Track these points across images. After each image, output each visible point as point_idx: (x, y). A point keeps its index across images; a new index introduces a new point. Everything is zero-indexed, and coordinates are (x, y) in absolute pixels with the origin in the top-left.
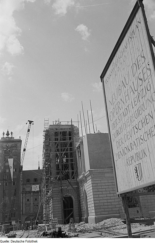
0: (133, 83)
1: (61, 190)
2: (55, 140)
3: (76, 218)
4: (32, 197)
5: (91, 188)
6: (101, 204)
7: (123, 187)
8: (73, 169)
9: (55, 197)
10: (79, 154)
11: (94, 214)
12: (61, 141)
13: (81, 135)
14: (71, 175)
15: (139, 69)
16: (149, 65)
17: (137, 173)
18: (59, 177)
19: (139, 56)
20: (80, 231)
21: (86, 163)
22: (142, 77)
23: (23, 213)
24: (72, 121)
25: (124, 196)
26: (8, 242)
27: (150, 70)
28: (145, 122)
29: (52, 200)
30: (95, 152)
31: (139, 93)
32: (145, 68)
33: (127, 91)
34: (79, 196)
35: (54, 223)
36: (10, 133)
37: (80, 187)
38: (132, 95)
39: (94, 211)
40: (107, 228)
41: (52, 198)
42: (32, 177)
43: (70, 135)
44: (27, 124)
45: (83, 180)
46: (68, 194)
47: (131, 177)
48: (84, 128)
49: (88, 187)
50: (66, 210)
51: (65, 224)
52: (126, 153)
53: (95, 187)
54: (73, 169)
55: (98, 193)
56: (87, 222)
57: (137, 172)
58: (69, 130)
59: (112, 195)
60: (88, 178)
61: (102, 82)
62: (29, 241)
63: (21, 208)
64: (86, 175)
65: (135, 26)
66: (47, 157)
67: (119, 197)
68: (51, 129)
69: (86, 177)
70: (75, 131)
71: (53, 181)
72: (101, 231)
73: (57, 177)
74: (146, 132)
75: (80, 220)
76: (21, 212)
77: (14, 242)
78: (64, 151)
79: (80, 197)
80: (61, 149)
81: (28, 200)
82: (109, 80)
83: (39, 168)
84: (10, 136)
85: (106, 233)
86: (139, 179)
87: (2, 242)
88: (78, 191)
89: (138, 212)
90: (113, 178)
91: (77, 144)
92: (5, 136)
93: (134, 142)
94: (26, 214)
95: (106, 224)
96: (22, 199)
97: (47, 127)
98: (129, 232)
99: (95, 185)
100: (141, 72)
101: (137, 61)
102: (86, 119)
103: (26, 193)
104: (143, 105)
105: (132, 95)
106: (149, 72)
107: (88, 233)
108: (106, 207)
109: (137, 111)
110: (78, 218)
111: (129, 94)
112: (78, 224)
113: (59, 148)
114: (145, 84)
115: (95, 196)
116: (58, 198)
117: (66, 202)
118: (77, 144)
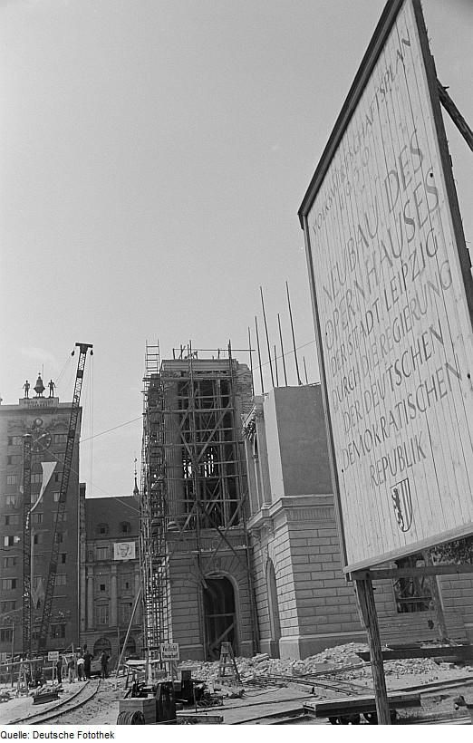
0: (389, 231)
1: (198, 557)
2: (180, 406)
3: (243, 642)
4: (114, 578)
5: (288, 553)
6: (317, 601)
7: (361, 553)
8: (233, 496)
9: (179, 579)
10: (252, 448)
11: (297, 631)
12: (197, 409)
13: (257, 392)
14: (228, 513)
15: (405, 188)
16: (432, 175)
17: (399, 509)
18: (192, 518)
19: (406, 147)
20: (253, 682)
21: (271, 477)
22: (413, 216)
23: (89, 627)
24: (230, 346)
25: (363, 576)
26: (24, 736)
27: (435, 192)
28: (419, 352)
29: (169, 587)
30: (301, 442)
31: (406, 264)
32: (422, 186)
33: (371, 257)
34: (251, 576)
35: (170, 657)
36: (45, 384)
37: (255, 550)
38: (385, 269)
39: (295, 622)
40: (334, 673)
41: (172, 582)
42: (110, 518)
43: (225, 390)
44: (73, 354)
45: (265, 528)
46: (218, 571)
47: (381, 520)
48: (266, 368)
49: (278, 549)
50: (213, 618)
51: (210, 658)
52: (370, 447)
53: (299, 551)
54: (233, 496)
55: (310, 567)
56: (276, 655)
57: (398, 505)
58: (223, 376)
59: (331, 575)
60: (280, 521)
61: (305, 228)
62: (88, 735)
63: (83, 612)
64: (274, 514)
65: (394, 55)
66: (154, 453)
67: (348, 580)
68: (165, 373)
69: (272, 519)
70: (241, 380)
71: (173, 530)
72: (315, 681)
73: (186, 518)
74: (423, 383)
75: (257, 649)
76: (83, 624)
77: (41, 735)
78: (206, 439)
79: (255, 580)
80: (199, 433)
81: (103, 587)
82: (324, 222)
83: (136, 491)
84: (46, 394)
85: (327, 687)
86: (403, 528)
87: (7, 736)
88: (248, 560)
89: (431, 624)
90: (334, 522)
91: (247, 419)
92: (32, 394)
93: (391, 414)
94: (96, 630)
95: (331, 662)
96: (83, 583)
97: (155, 367)
98: (377, 686)
99: (299, 543)
100: (412, 198)
101: (401, 164)
102: (275, 341)
103: (97, 564)
104: (416, 300)
105: (385, 269)
106: (431, 196)
107: (274, 689)
108: (334, 609)
109: (399, 318)
110: (251, 642)
111: (378, 267)
112: (248, 660)
113: (192, 430)
114: (421, 235)
115: (301, 577)
116: (188, 583)
117: (214, 596)
118: (247, 419)
